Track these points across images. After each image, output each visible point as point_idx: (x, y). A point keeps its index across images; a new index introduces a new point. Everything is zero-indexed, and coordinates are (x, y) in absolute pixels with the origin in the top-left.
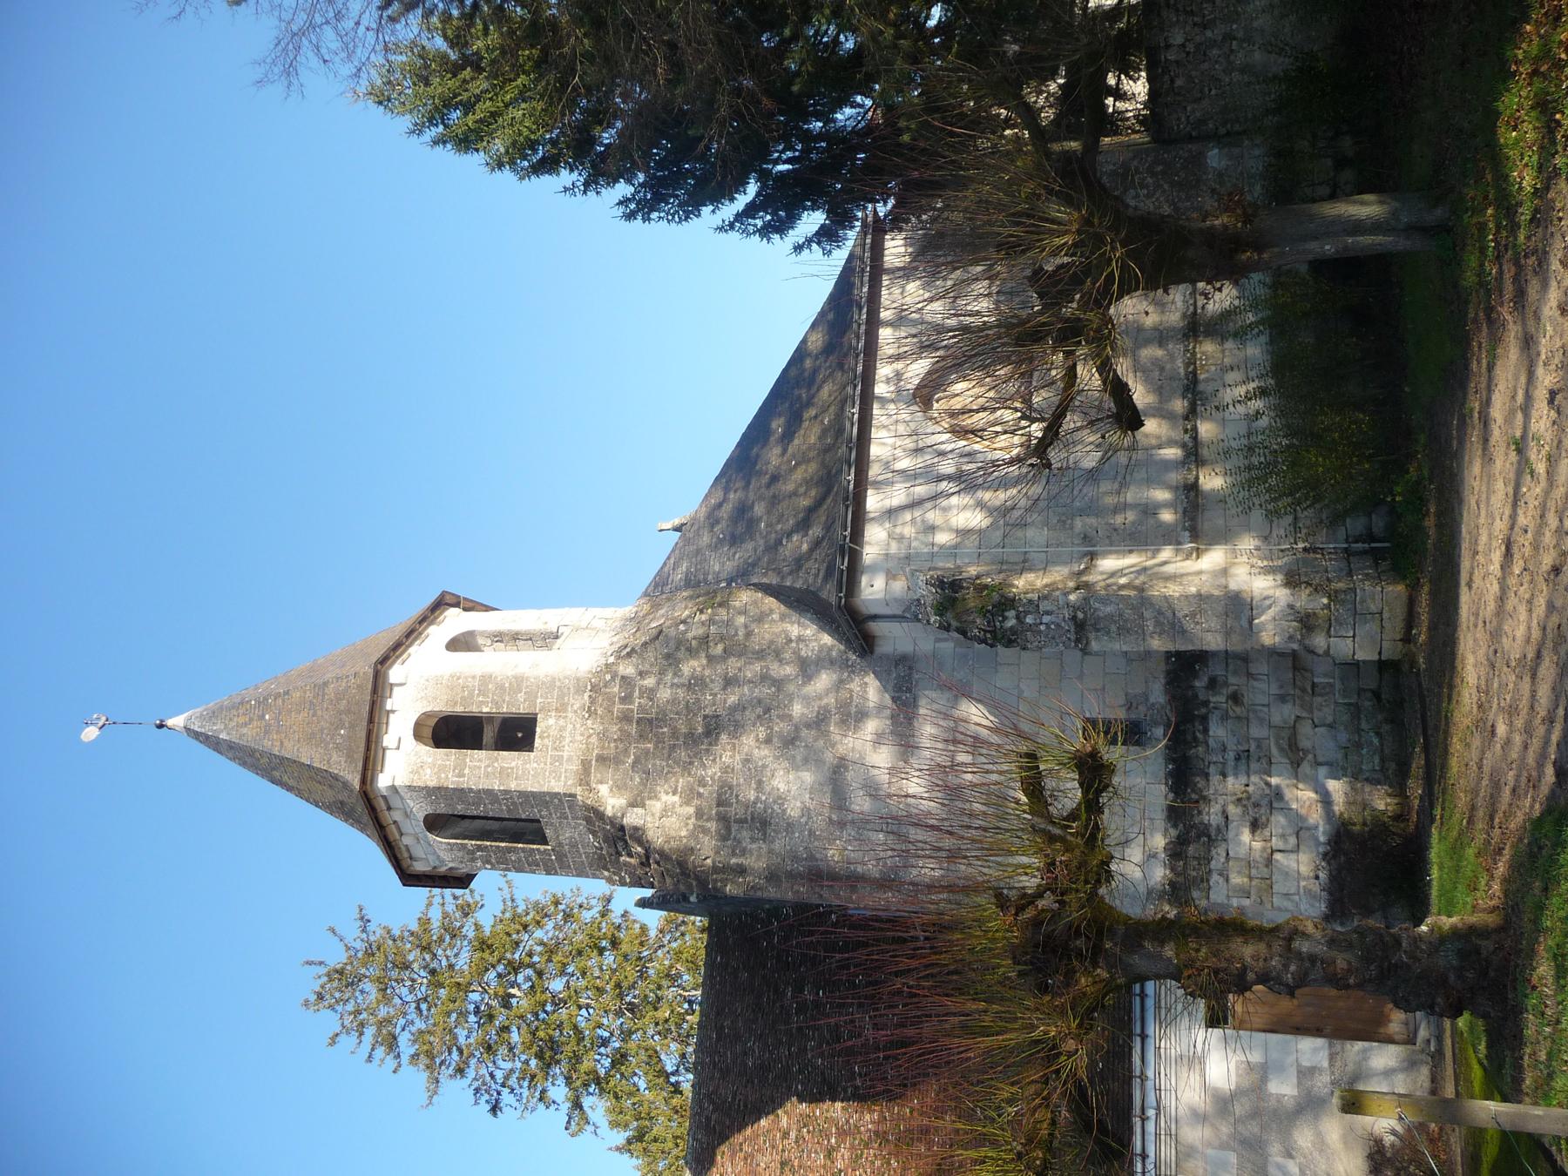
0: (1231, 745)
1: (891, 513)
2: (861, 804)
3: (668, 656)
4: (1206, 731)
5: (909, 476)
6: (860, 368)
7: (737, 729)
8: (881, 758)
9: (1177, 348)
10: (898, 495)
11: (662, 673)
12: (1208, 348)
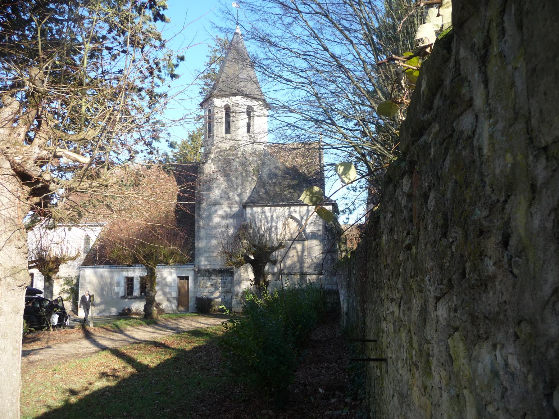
0: (227, 281)
1: (264, 212)
2: (213, 209)
3: (243, 163)
4: (229, 276)
5: (272, 217)
6: (295, 203)
7: (227, 181)
8: (220, 212)
9: (299, 271)
10: (268, 214)
11: (239, 162)
12: (298, 277)
